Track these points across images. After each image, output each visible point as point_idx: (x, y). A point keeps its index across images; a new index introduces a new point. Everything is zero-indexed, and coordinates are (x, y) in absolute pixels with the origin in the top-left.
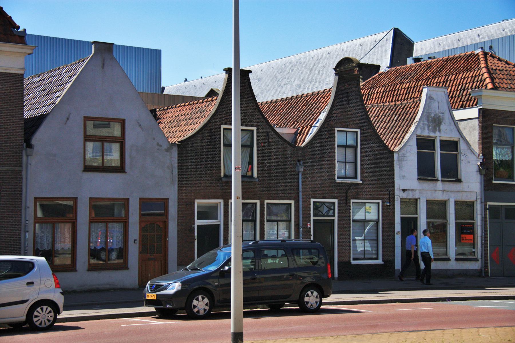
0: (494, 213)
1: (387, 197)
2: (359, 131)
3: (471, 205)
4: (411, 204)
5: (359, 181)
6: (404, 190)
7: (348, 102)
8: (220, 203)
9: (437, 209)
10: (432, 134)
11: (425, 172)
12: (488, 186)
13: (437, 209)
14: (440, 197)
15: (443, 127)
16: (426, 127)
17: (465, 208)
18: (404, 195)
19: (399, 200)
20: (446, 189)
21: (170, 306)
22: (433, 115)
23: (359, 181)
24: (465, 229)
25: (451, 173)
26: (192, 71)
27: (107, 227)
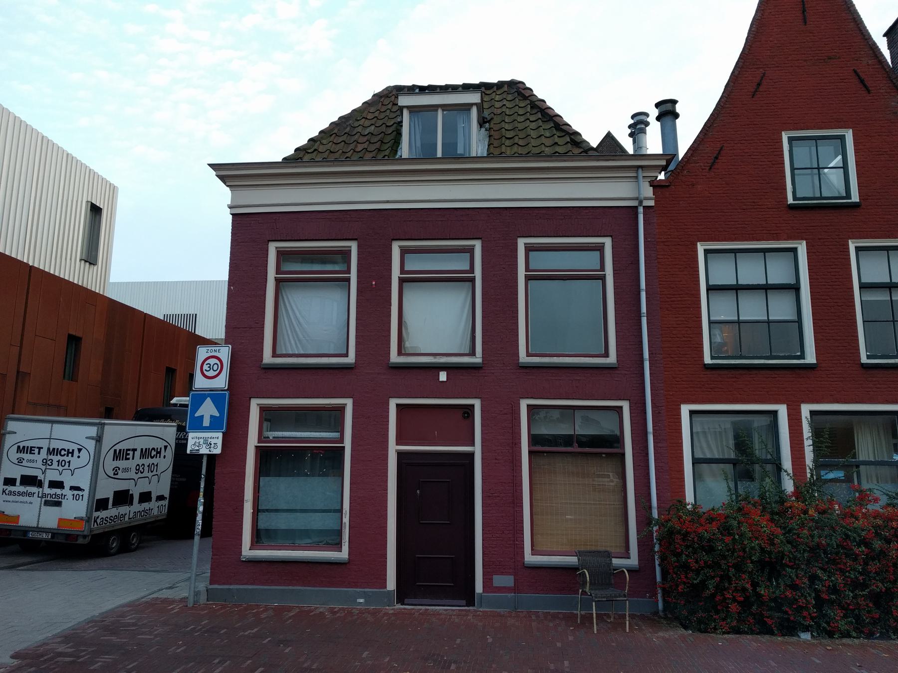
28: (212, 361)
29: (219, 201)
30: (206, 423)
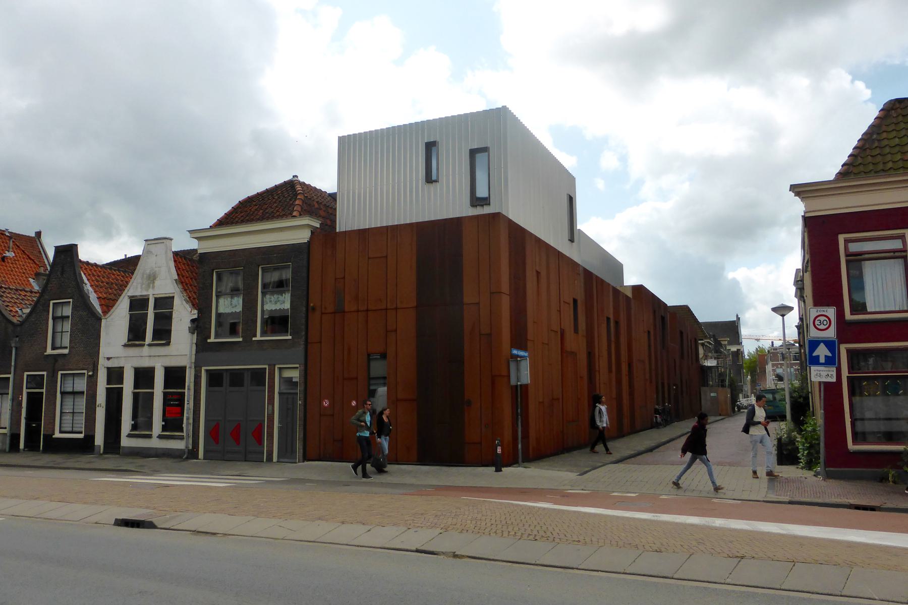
0: (215, 379)
1: (91, 366)
2: (52, 302)
3: (182, 370)
4: (115, 375)
5: (49, 351)
6: (108, 359)
7: (62, 274)
8: (207, 371)
9: (144, 376)
10: (144, 293)
11: (136, 334)
12: (203, 347)
13: (144, 376)
14: (145, 363)
15: (157, 283)
16: (139, 286)
17: (174, 376)
18: (111, 364)
19: (105, 371)
20: (152, 354)
21: (362, 434)
22: (148, 272)
23: (49, 351)
24: (174, 403)
25: (163, 334)
26: (630, 280)
27: (374, 378)
28: (822, 318)
29: (798, 208)
30: (822, 360)
